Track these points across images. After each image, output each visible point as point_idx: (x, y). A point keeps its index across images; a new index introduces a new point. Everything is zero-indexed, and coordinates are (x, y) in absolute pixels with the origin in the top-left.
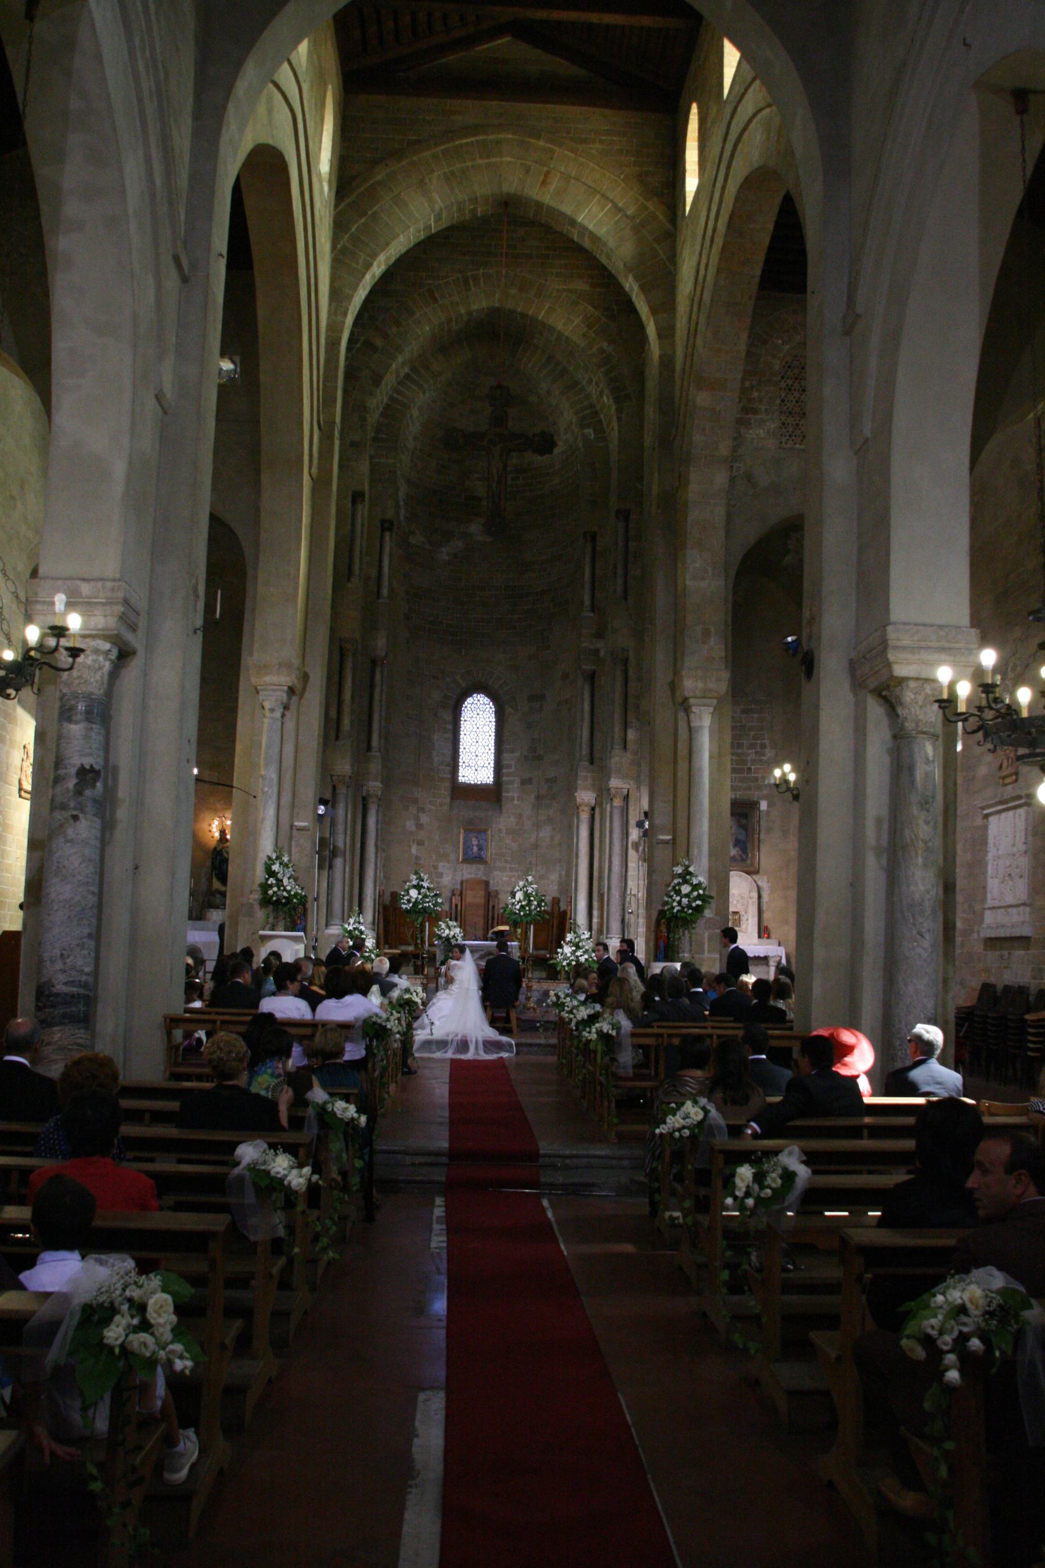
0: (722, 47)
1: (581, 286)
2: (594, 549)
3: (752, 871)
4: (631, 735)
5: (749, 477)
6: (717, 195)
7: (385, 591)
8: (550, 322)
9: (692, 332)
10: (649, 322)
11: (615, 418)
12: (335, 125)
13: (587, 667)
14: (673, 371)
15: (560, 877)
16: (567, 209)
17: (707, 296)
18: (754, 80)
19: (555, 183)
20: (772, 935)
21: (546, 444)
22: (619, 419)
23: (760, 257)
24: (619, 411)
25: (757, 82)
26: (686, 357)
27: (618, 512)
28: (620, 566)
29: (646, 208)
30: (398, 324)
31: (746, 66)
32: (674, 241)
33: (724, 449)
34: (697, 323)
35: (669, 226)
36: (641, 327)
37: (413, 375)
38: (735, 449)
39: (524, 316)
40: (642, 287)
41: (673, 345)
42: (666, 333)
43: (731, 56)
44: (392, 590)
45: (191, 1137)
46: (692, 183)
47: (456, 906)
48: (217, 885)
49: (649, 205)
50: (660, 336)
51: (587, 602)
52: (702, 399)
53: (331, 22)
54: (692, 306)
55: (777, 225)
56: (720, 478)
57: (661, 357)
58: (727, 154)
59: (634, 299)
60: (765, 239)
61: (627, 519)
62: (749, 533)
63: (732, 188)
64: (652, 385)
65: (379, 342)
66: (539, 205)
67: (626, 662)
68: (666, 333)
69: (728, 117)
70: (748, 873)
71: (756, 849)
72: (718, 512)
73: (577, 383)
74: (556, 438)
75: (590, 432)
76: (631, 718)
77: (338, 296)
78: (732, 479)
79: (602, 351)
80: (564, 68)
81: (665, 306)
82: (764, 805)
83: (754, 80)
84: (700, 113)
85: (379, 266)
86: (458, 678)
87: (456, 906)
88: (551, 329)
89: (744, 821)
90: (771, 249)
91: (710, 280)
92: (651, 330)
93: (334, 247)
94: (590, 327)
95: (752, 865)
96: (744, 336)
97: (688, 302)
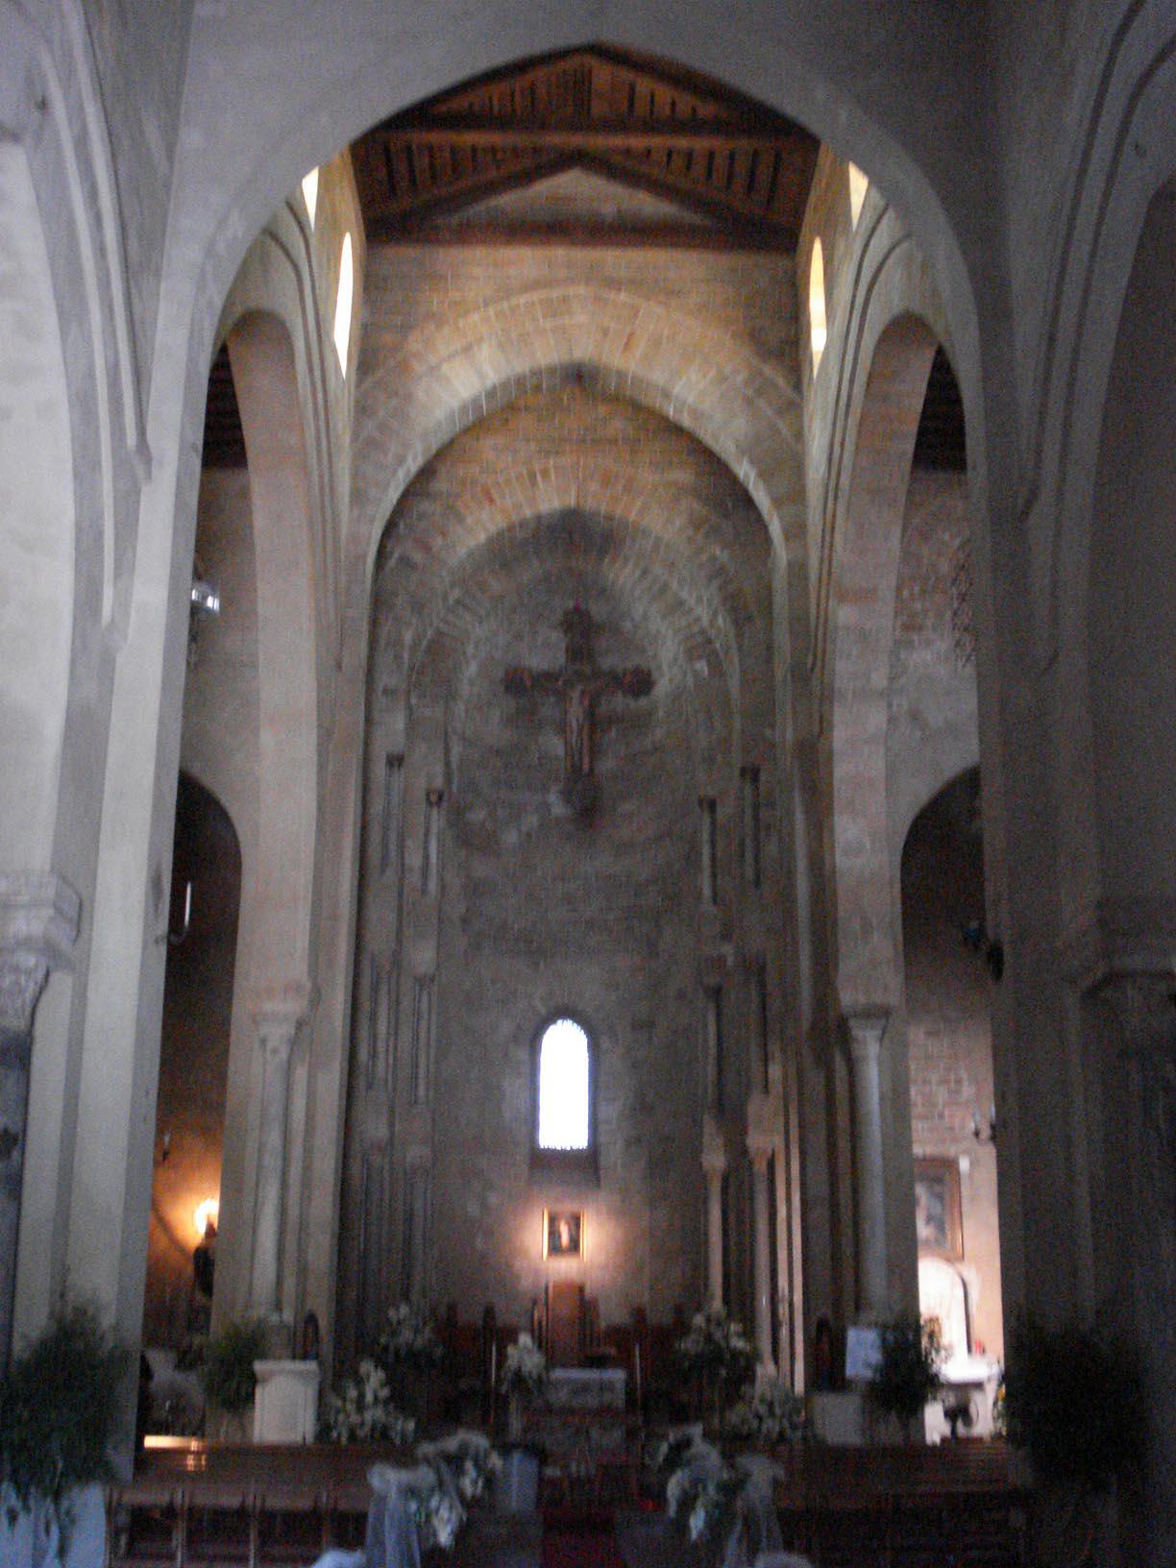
0: (847, 172)
1: (684, 476)
2: (713, 823)
3: (955, 1257)
4: (775, 1071)
5: (915, 716)
6: (850, 352)
7: (433, 885)
8: (645, 522)
9: (828, 525)
10: (771, 519)
11: (735, 646)
12: (355, 271)
13: (711, 980)
14: (806, 579)
15: (684, 1274)
16: (658, 377)
17: (845, 481)
18: (885, 209)
19: (640, 348)
20: (987, 1349)
21: (641, 683)
22: (740, 649)
23: (913, 428)
24: (739, 636)
25: (890, 214)
26: (822, 560)
27: (743, 771)
28: (748, 842)
29: (761, 374)
30: (444, 534)
31: (874, 193)
32: (800, 416)
33: (879, 680)
34: (834, 516)
35: (790, 393)
36: (764, 527)
37: (467, 601)
38: (892, 679)
39: (610, 518)
40: (760, 475)
41: (805, 547)
42: (796, 531)
43: (858, 184)
44: (443, 887)
45: (99, 381)
46: (819, 338)
47: (540, 1323)
48: (200, 1297)
49: (767, 370)
50: (788, 536)
51: (707, 892)
52: (844, 615)
53: (346, 152)
54: (827, 492)
55: (931, 385)
56: (876, 718)
57: (790, 564)
58: (860, 301)
59: (751, 488)
60: (917, 404)
61: (755, 779)
62: (919, 791)
63: (869, 341)
64: (780, 601)
65: (418, 557)
66: (621, 375)
67: (762, 969)
68: (796, 531)
69: (859, 252)
70: (948, 1260)
71: (958, 1226)
72: (876, 765)
73: (681, 603)
74: (655, 675)
75: (702, 666)
76: (774, 1049)
77: (358, 496)
78: (892, 720)
79: (713, 559)
80: (647, 205)
81: (793, 496)
82: (964, 1164)
83: (885, 209)
84: (824, 249)
85: (415, 459)
86: (538, 1003)
87: (540, 1323)
88: (646, 534)
89: (937, 1188)
90: (925, 416)
91: (847, 462)
92: (775, 529)
93: (355, 436)
94: (697, 528)
95: (954, 1248)
96: (896, 531)
97: (821, 490)
